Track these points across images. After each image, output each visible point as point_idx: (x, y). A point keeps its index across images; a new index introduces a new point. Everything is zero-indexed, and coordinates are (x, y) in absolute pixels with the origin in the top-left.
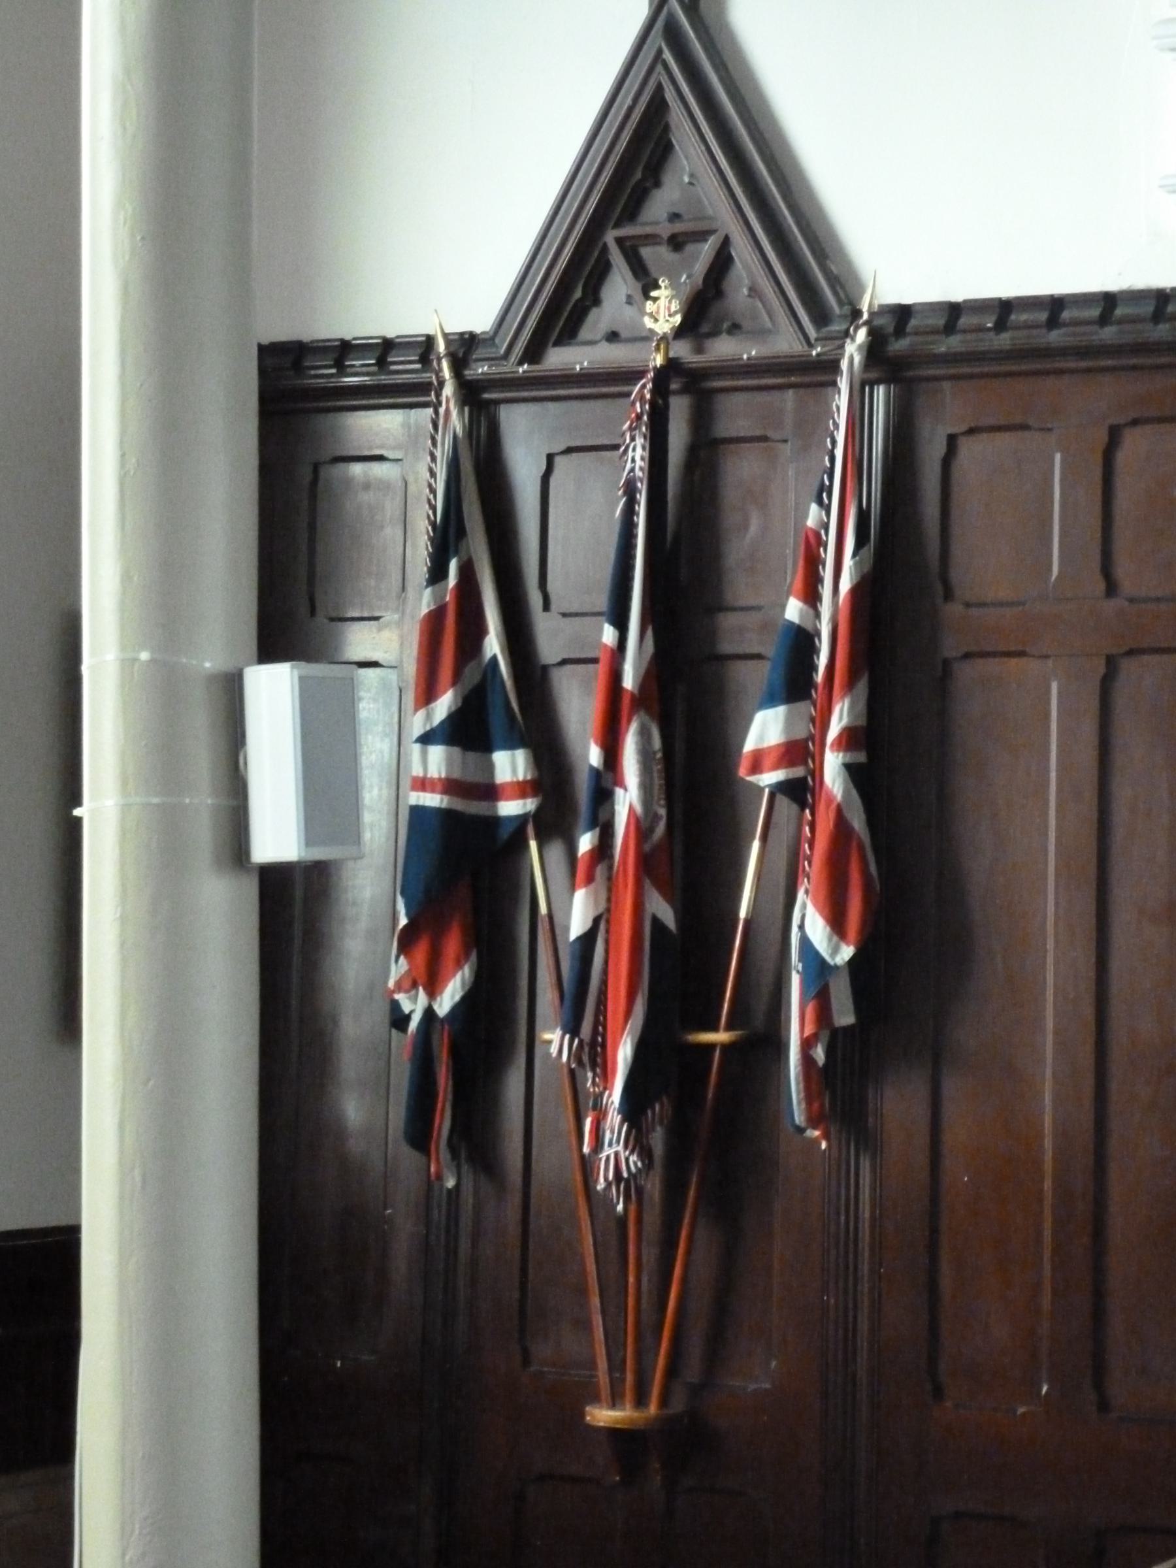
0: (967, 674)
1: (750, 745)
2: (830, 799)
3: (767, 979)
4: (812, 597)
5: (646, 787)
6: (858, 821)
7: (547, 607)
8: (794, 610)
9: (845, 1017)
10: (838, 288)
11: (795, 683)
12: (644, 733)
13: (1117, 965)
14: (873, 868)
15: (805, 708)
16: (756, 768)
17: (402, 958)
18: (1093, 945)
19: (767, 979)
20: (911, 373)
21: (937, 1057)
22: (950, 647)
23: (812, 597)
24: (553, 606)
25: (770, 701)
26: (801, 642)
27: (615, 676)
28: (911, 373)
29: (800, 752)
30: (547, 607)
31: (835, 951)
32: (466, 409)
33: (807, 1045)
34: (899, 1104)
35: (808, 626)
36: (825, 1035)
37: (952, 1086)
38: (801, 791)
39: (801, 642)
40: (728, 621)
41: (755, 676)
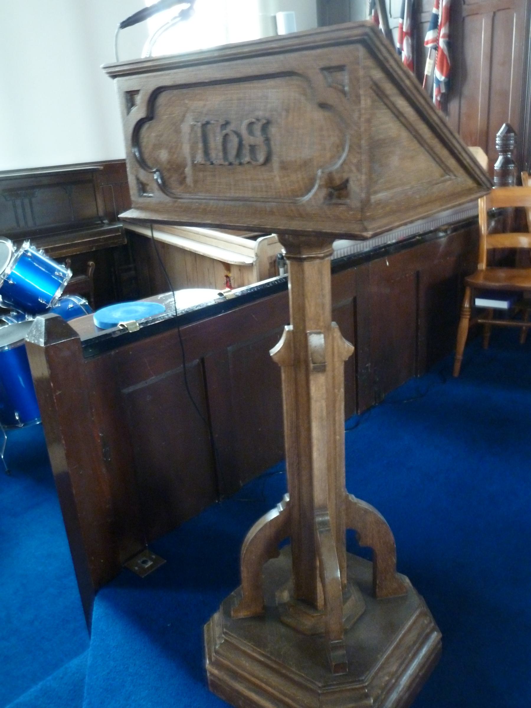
0: (468, 20)
1: (426, 40)
2: (440, 48)
3: (431, 87)
4: (438, 7)
5: (408, 51)
6: (446, 52)
7: (391, 17)
8: (434, 11)
9: (443, 90)
10: (415, 31)
11: (435, 26)
12: (407, 40)
13: (493, 74)
14: (449, 61)
15: (437, 30)
16: (427, 43)
17: (99, 610)
18: (489, 69)
19: (431, 87)
20: (526, 153)
21: (460, 95)
22: (464, 14)
23: (438, 7)
24: (392, 16)
25: (430, 30)
26: (436, 17)
27: (402, 28)
28: (526, 153)
29: (436, 40)
30: (391, 17)
31: (441, 78)
32: (102, 168)
33: (436, 96)
34: (453, 106)
35: (437, 13)
36: (440, 95)
37: (463, 101)
38: (436, 48)
39: (436, 17)
40: (423, 15)
41: (427, 26)
